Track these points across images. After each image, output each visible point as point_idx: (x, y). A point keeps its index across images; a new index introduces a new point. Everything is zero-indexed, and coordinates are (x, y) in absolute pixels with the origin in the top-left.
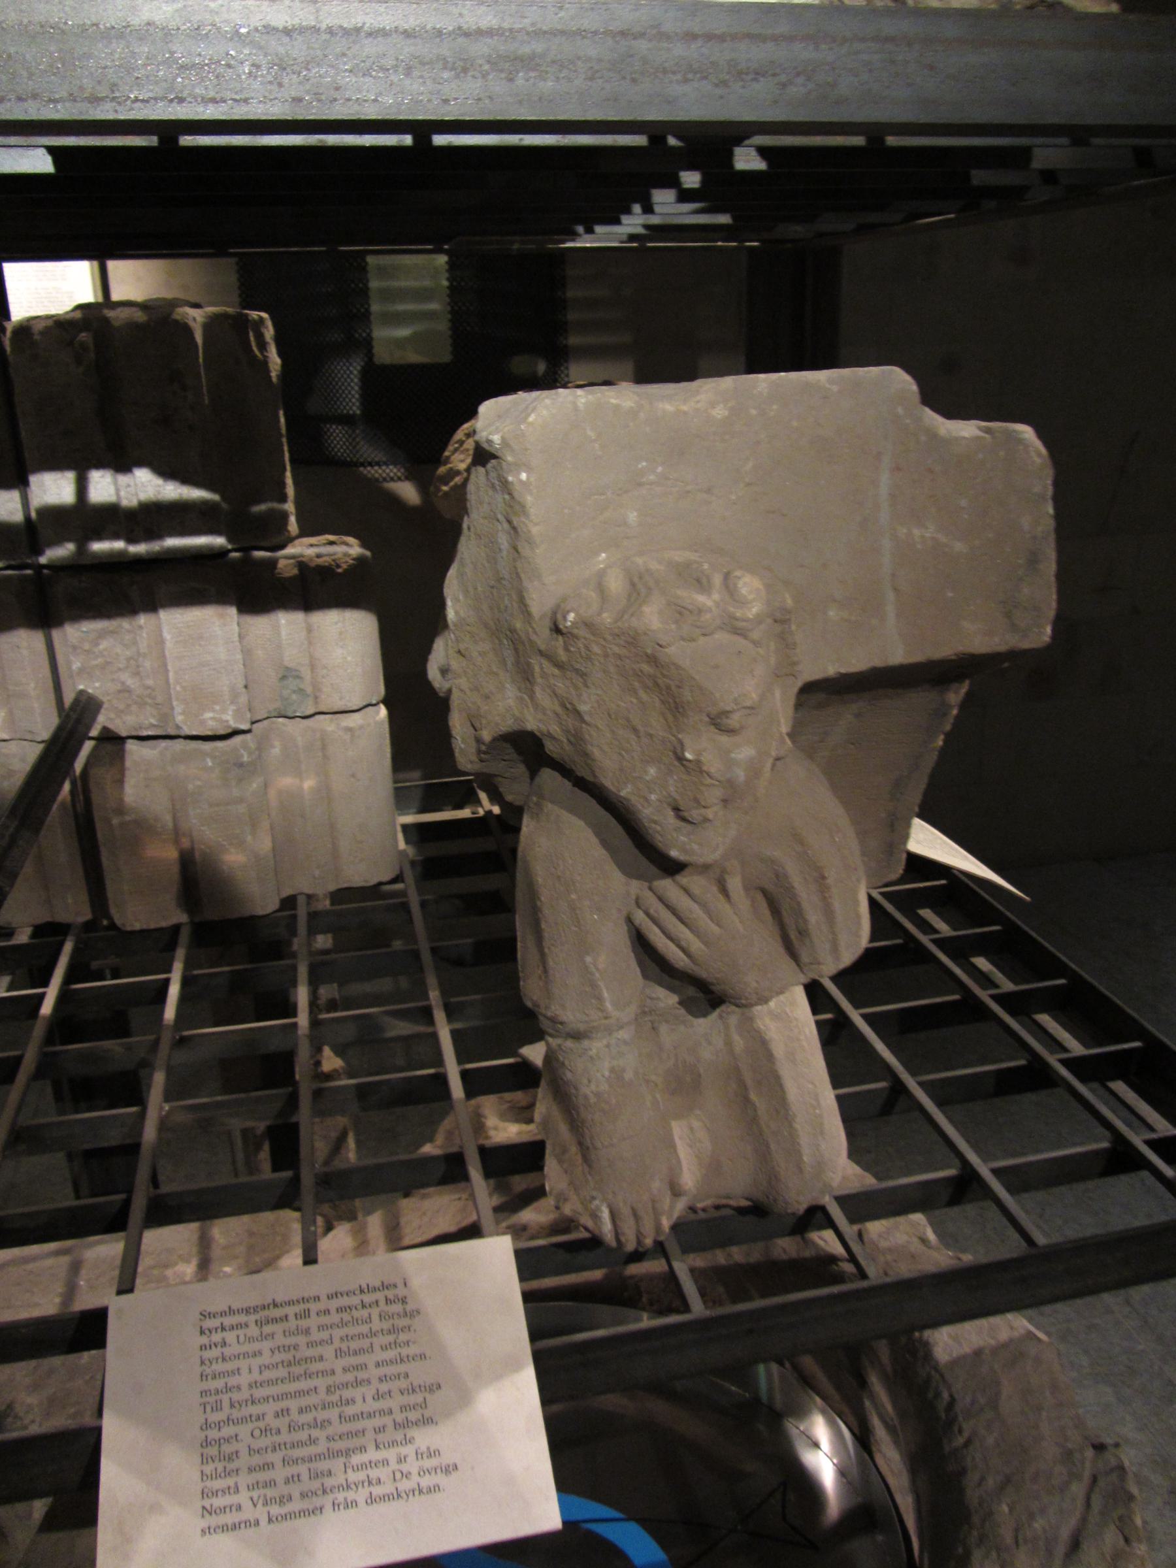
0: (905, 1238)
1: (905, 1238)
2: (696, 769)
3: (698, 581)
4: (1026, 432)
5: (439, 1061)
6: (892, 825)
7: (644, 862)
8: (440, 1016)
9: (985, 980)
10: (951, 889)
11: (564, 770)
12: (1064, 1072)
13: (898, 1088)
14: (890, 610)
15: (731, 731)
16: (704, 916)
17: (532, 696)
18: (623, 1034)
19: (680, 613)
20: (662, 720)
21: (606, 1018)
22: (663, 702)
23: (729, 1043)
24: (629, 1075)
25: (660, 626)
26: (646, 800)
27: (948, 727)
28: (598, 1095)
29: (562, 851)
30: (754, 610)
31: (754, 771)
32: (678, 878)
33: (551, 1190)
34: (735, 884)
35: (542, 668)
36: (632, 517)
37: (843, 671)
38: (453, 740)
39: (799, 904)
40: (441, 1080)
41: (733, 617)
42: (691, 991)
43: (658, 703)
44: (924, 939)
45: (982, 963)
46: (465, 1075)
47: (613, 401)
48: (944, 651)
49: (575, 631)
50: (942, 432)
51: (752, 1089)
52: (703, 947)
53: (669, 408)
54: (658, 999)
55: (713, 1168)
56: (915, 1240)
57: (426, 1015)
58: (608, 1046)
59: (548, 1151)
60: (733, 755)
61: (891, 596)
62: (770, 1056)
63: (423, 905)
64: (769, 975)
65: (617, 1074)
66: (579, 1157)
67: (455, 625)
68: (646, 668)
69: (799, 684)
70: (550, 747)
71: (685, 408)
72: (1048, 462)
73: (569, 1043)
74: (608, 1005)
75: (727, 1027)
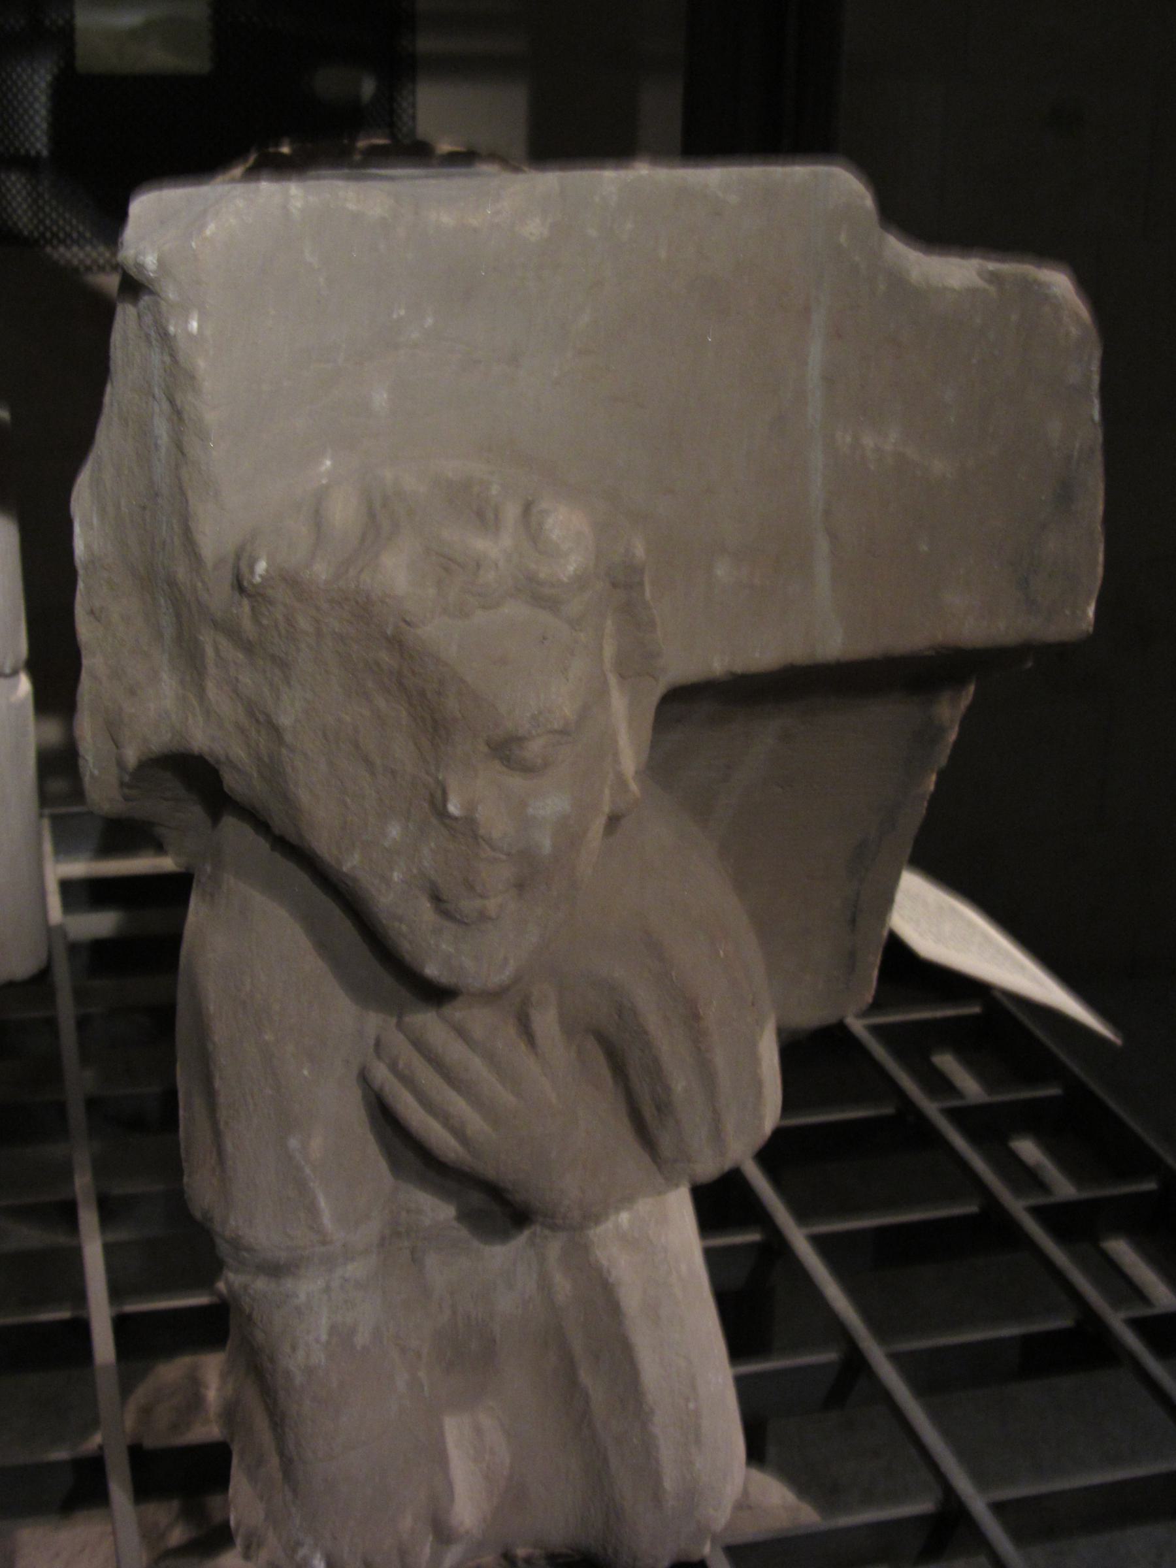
2: (466, 830)
3: (480, 515)
4: (1059, 282)
5: (80, 1296)
6: (853, 921)
7: (388, 981)
8: (88, 1219)
9: (1025, 1178)
10: (992, 1018)
11: (261, 825)
12: (1131, 1340)
13: (855, 1364)
14: (823, 572)
15: (527, 769)
18: (355, 1269)
19: (446, 569)
21: (324, 1243)
23: (545, 1283)
24: (362, 1338)
26: (386, 880)
27: (943, 760)
28: (310, 1371)
29: (250, 956)
30: (572, 566)
31: (570, 836)
32: (447, 1010)
33: (238, 1524)
34: (546, 1022)
35: (217, 650)
36: (380, 398)
38: (81, 762)
39: (656, 1060)
40: (80, 1329)
41: (531, 578)
42: (477, 1199)
44: (931, 1108)
45: (1028, 1149)
46: (121, 1324)
47: (351, 206)
48: (915, 636)
49: (270, 592)
50: (915, 276)
53: (447, 219)
55: (512, 1496)
57: (67, 1214)
59: (235, 1461)
61: (823, 546)
62: (614, 1308)
63: (82, 1023)
66: (279, 1475)
67: (86, 568)
68: (384, 657)
69: (660, 690)
70: (231, 781)
71: (474, 222)
72: (1094, 334)
73: (261, 1284)
74: (327, 1220)
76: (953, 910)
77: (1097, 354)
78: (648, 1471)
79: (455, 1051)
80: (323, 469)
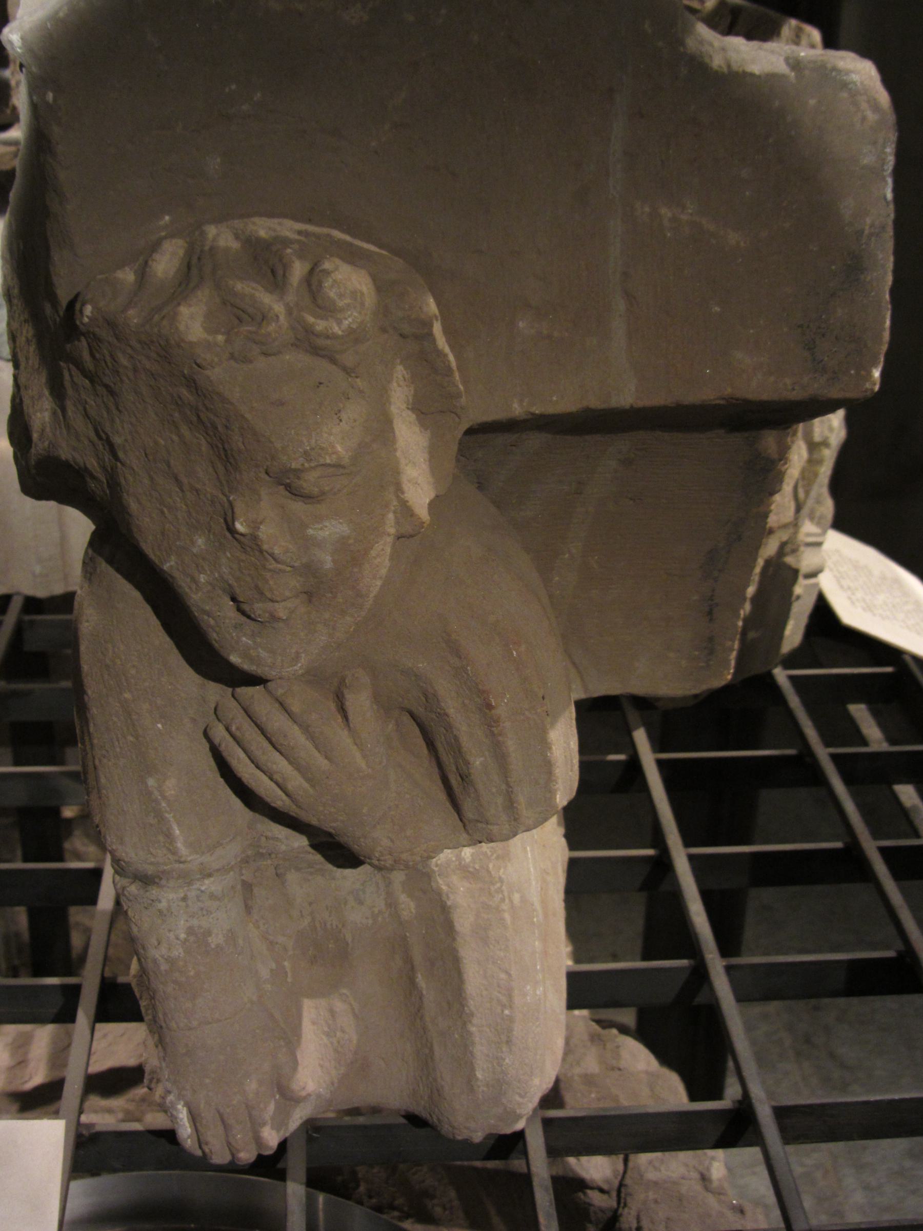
0: (682, 1170)
1: (682, 1170)
6: (710, 613)
16: (309, 745)
17: (63, 410)
20: (211, 470)
22: (212, 446)
23: (392, 904)
24: (216, 940)
25: (204, 335)
26: (195, 581)
28: (171, 961)
34: (360, 702)
37: (537, 410)
39: (456, 739)
41: (309, 331)
43: (204, 448)
50: (717, 62)
51: (424, 969)
52: (306, 785)
54: (277, 839)
55: (358, 1066)
56: (695, 1175)
58: (184, 899)
60: (310, 532)
62: (449, 928)
64: (409, 832)
65: (198, 939)
69: (465, 426)
74: (179, 845)
75: (389, 884)
76: (897, 581)
77: (893, 136)
78: (464, 1062)
79: (277, 721)
80: (162, 223)
